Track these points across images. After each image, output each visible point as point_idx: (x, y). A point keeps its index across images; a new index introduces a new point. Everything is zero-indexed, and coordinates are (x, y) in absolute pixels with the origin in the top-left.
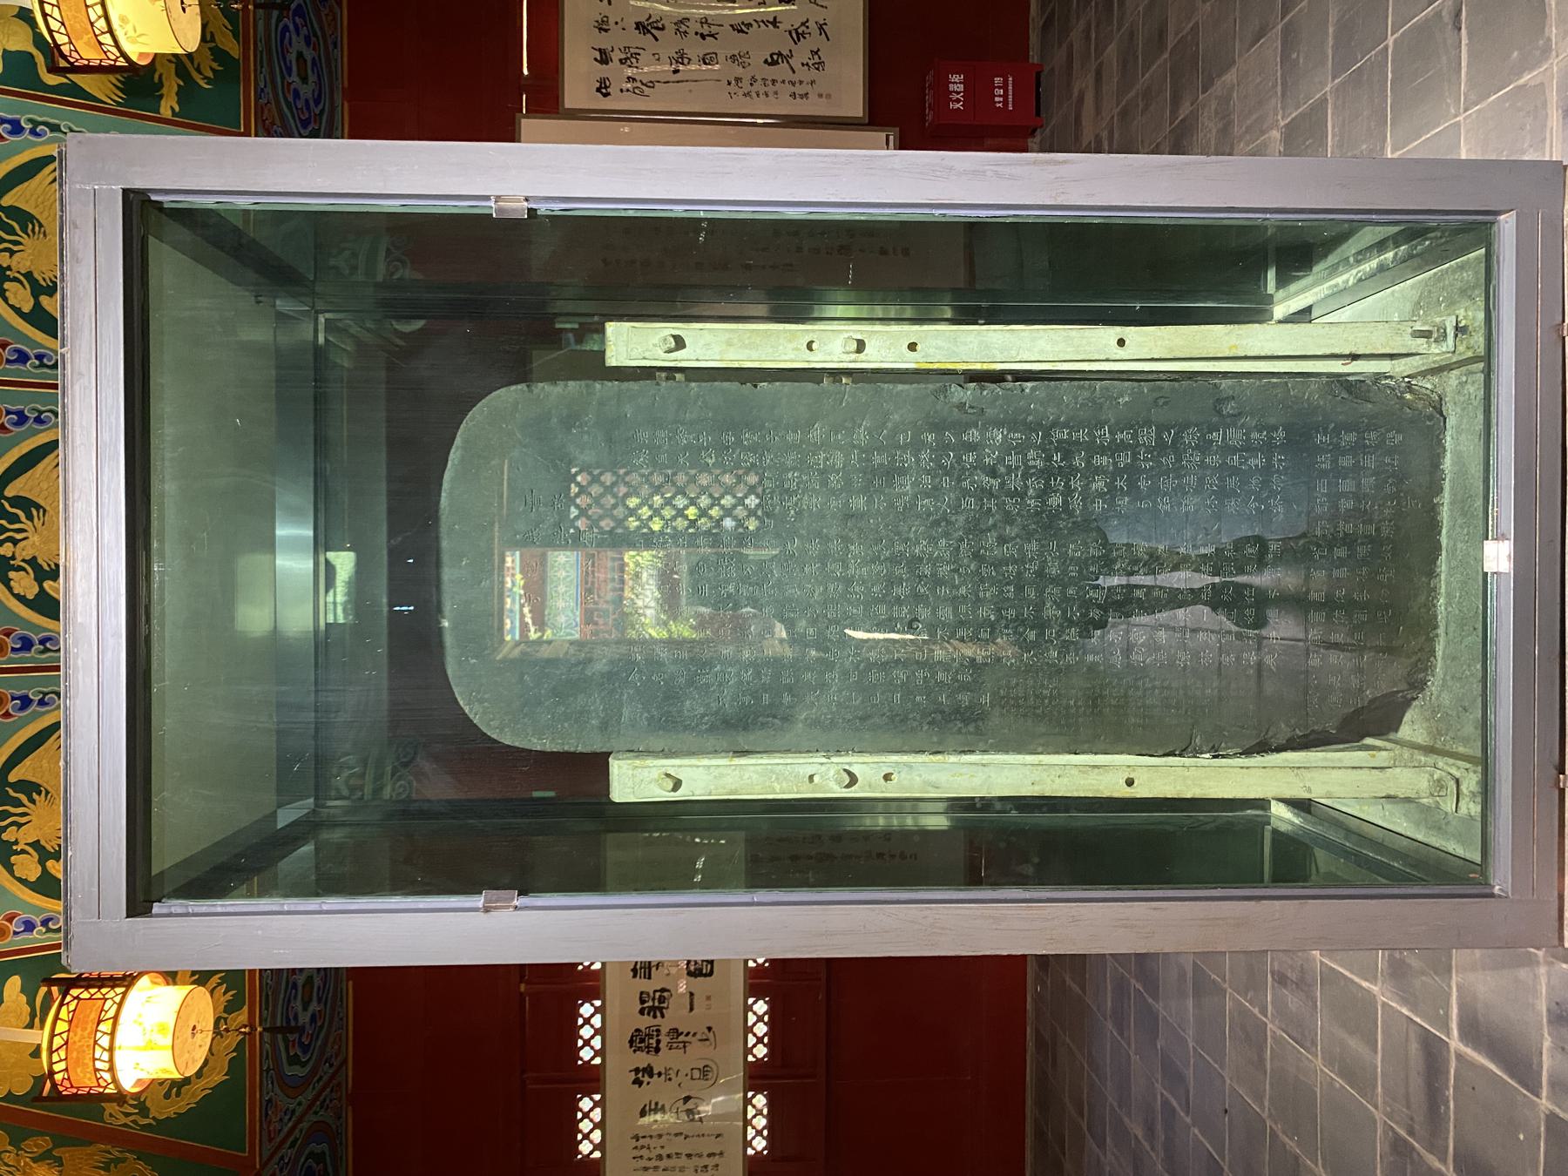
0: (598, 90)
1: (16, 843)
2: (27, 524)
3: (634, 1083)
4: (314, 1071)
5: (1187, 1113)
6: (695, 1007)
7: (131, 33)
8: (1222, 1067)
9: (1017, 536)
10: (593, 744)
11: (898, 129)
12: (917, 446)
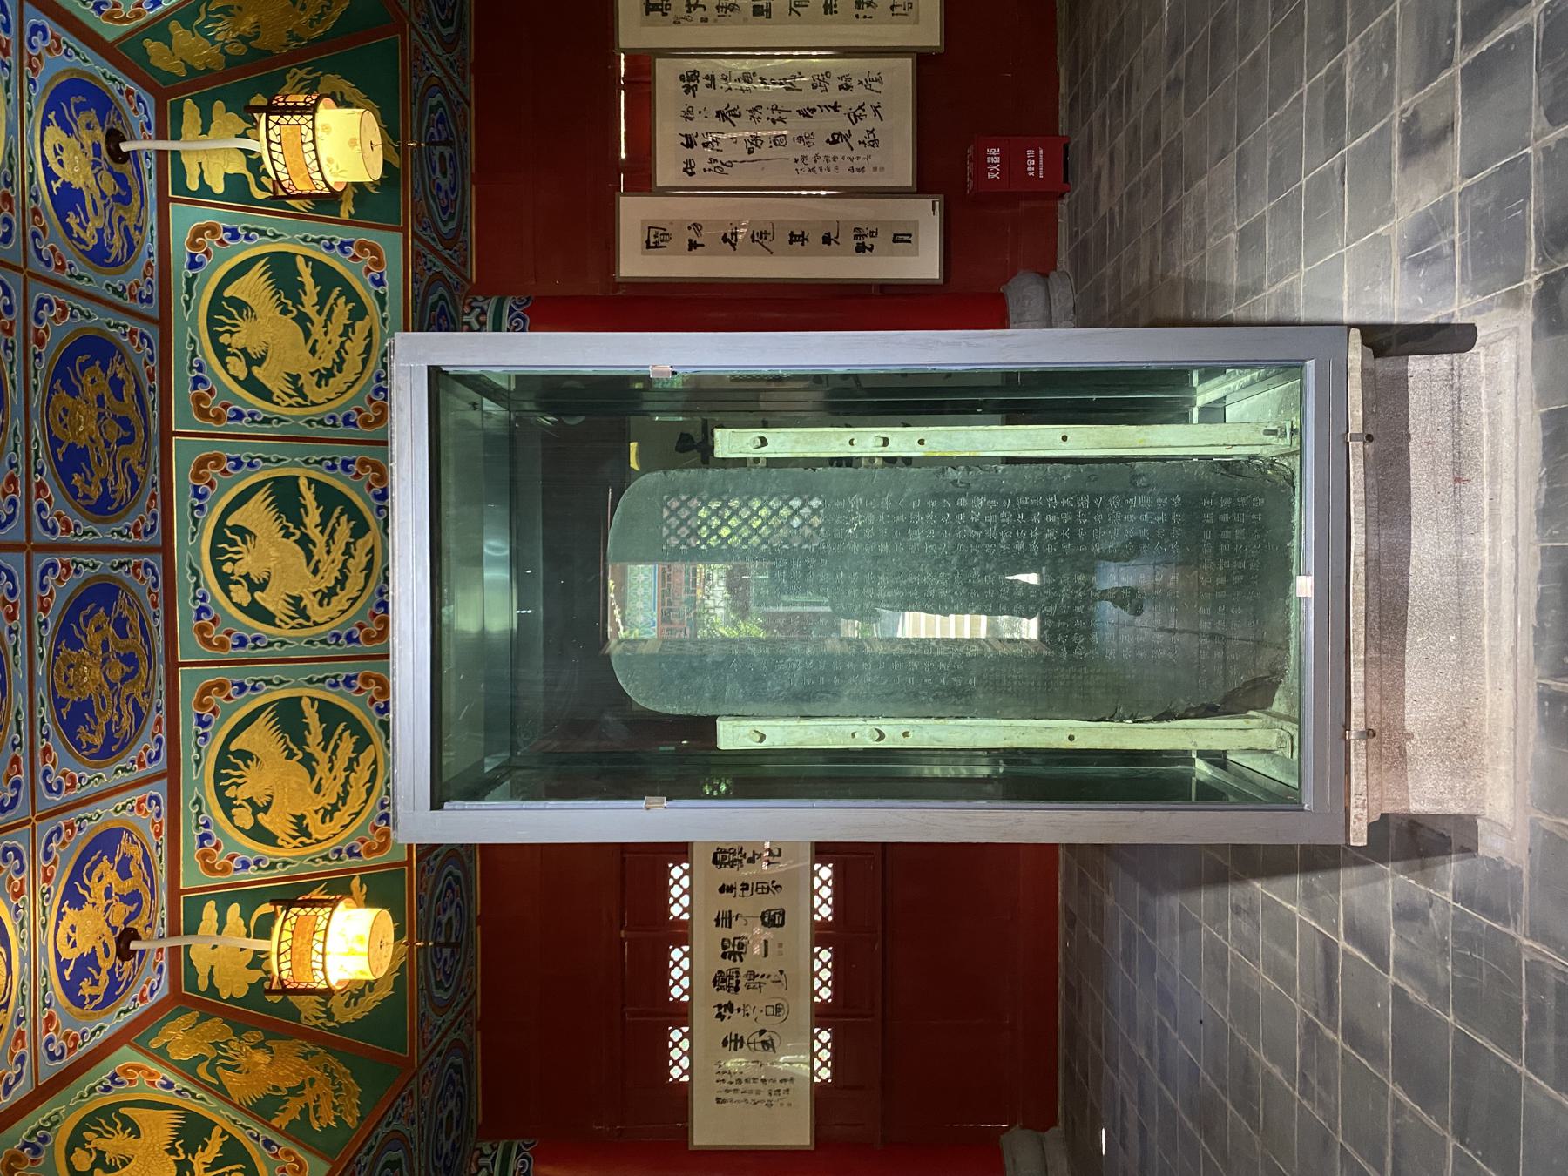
0: (685, 170)
1: (236, 799)
2: (242, 547)
3: (717, 1017)
4: (452, 999)
5: (1175, 1029)
6: (769, 953)
7: (334, 170)
8: (1199, 988)
9: (994, 570)
10: (703, 710)
11: (942, 196)
12: (924, 510)
